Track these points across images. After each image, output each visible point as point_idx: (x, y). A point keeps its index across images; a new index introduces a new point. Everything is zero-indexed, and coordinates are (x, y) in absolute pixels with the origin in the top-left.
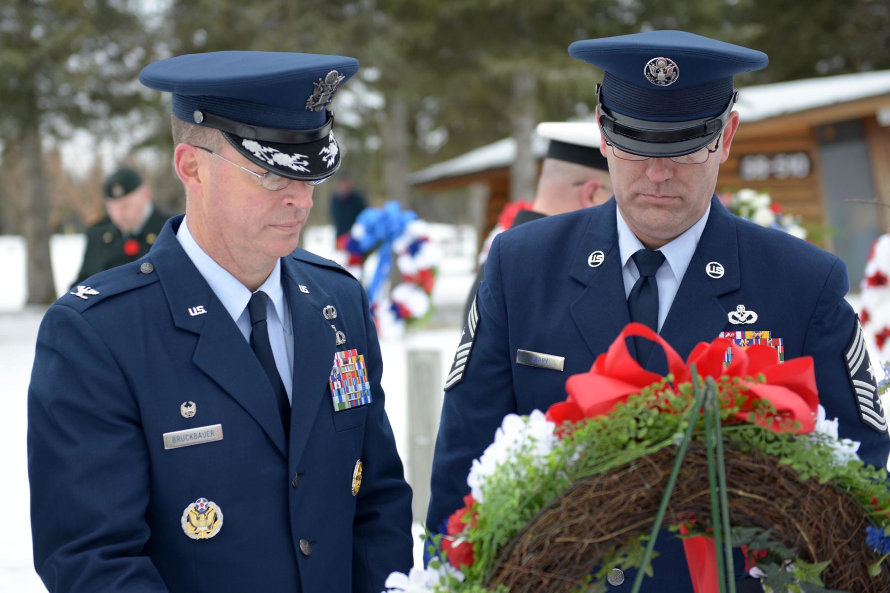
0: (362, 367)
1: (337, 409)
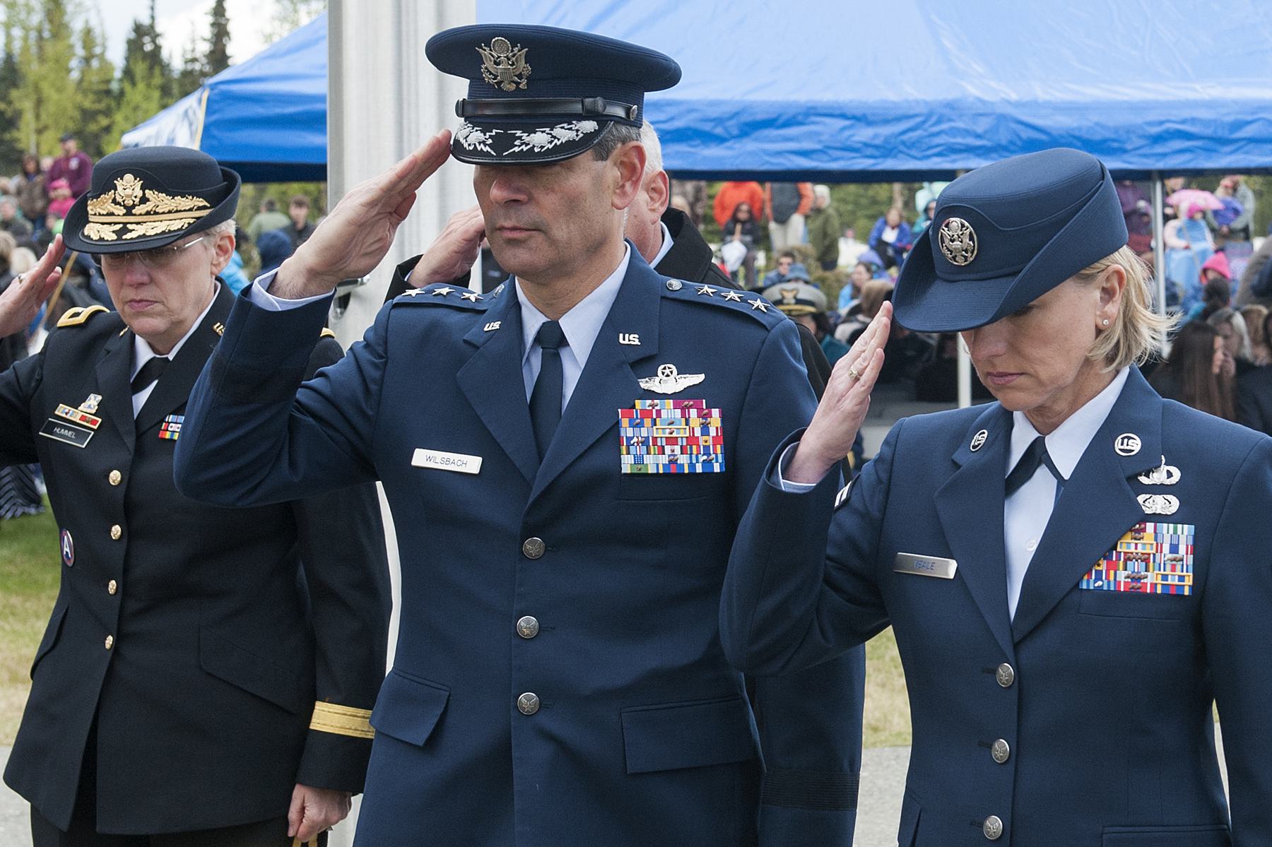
0: (713, 432)
1: (626, 469)
